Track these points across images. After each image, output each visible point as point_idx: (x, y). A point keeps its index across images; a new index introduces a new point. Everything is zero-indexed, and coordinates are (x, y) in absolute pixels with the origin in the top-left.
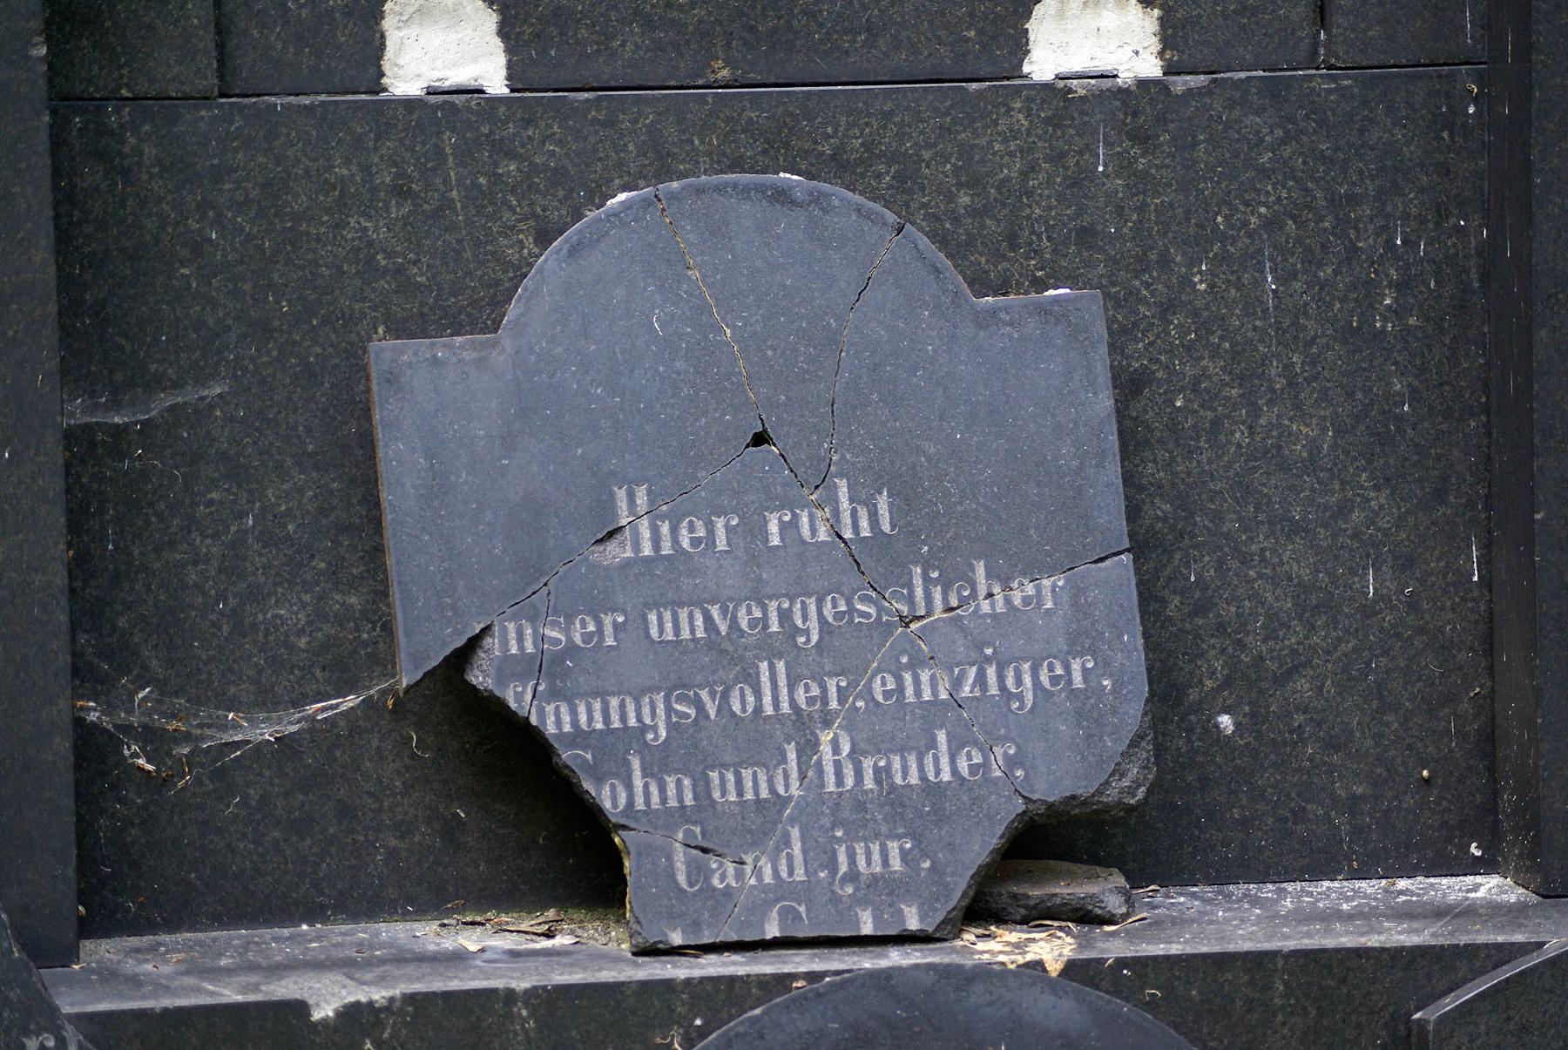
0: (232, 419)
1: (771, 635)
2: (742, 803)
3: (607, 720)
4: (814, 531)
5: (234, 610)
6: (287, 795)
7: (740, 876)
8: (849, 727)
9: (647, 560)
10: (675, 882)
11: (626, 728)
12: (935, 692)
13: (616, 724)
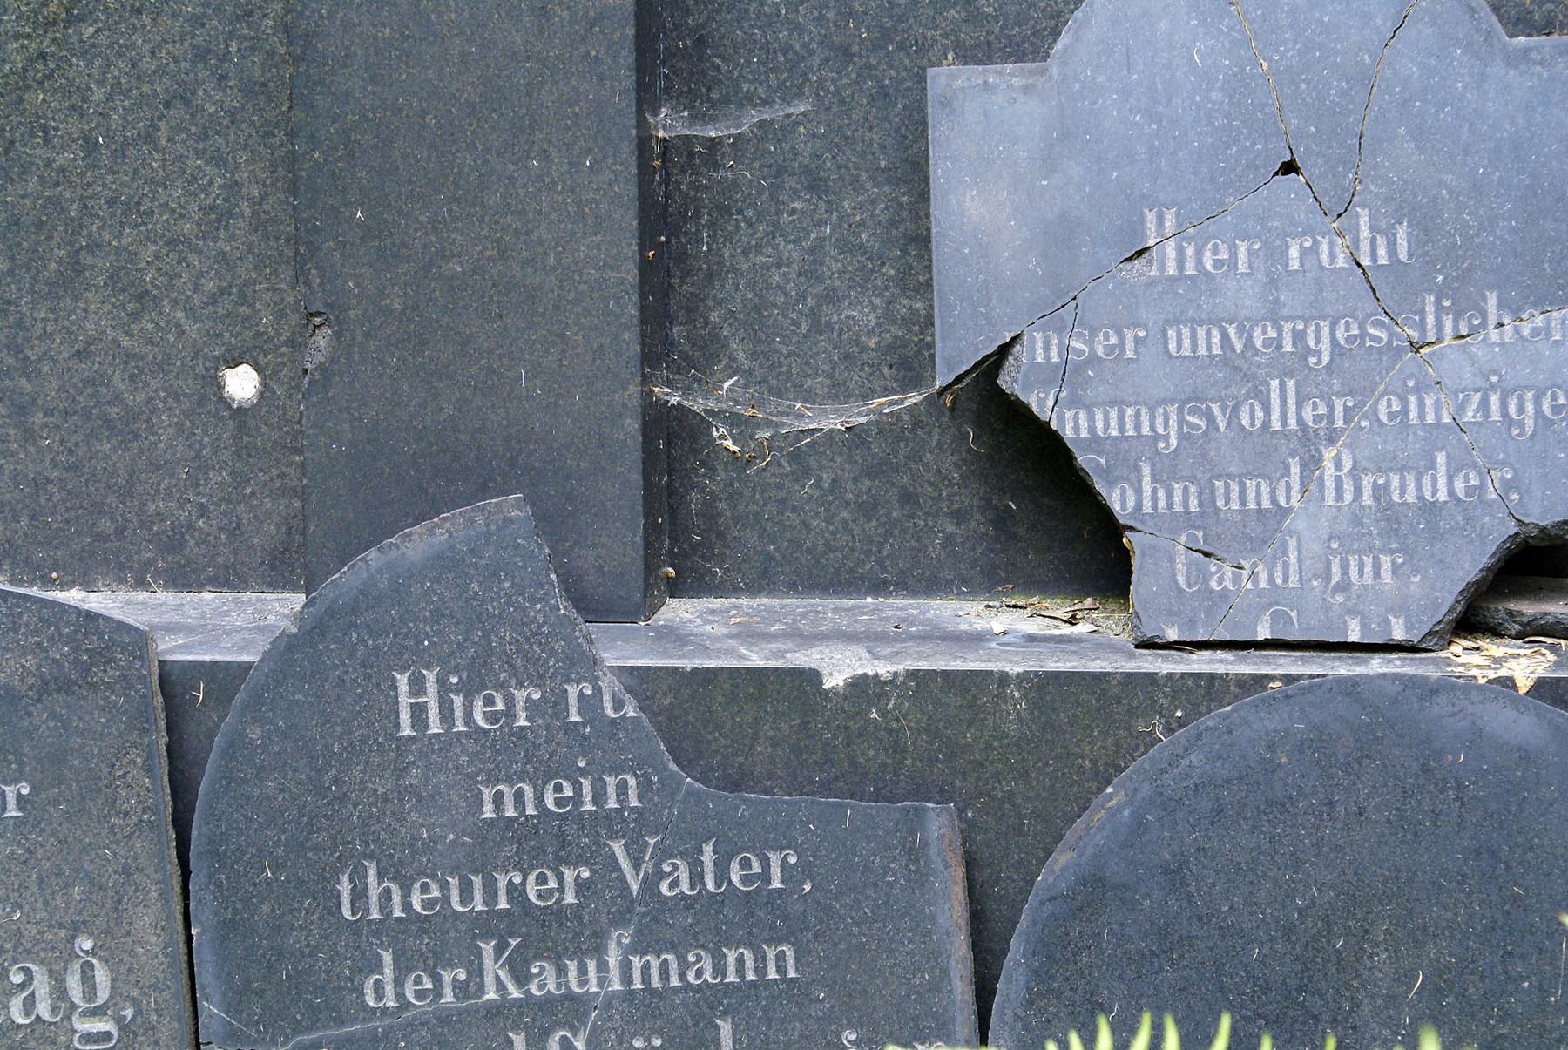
0: (814, 135)
1: (1283, 355)
2: (1244, 512)
3: (1122, 428)
4: (1333, 257)
5: (812, 310)
6: (855, 480)
7: (1237, 580)
8: (1351, 446)
9: (1172, 279)
10: (1176, 582)
11: (1139, 436)
12: (1438, 416)
13: (1131, 433)
